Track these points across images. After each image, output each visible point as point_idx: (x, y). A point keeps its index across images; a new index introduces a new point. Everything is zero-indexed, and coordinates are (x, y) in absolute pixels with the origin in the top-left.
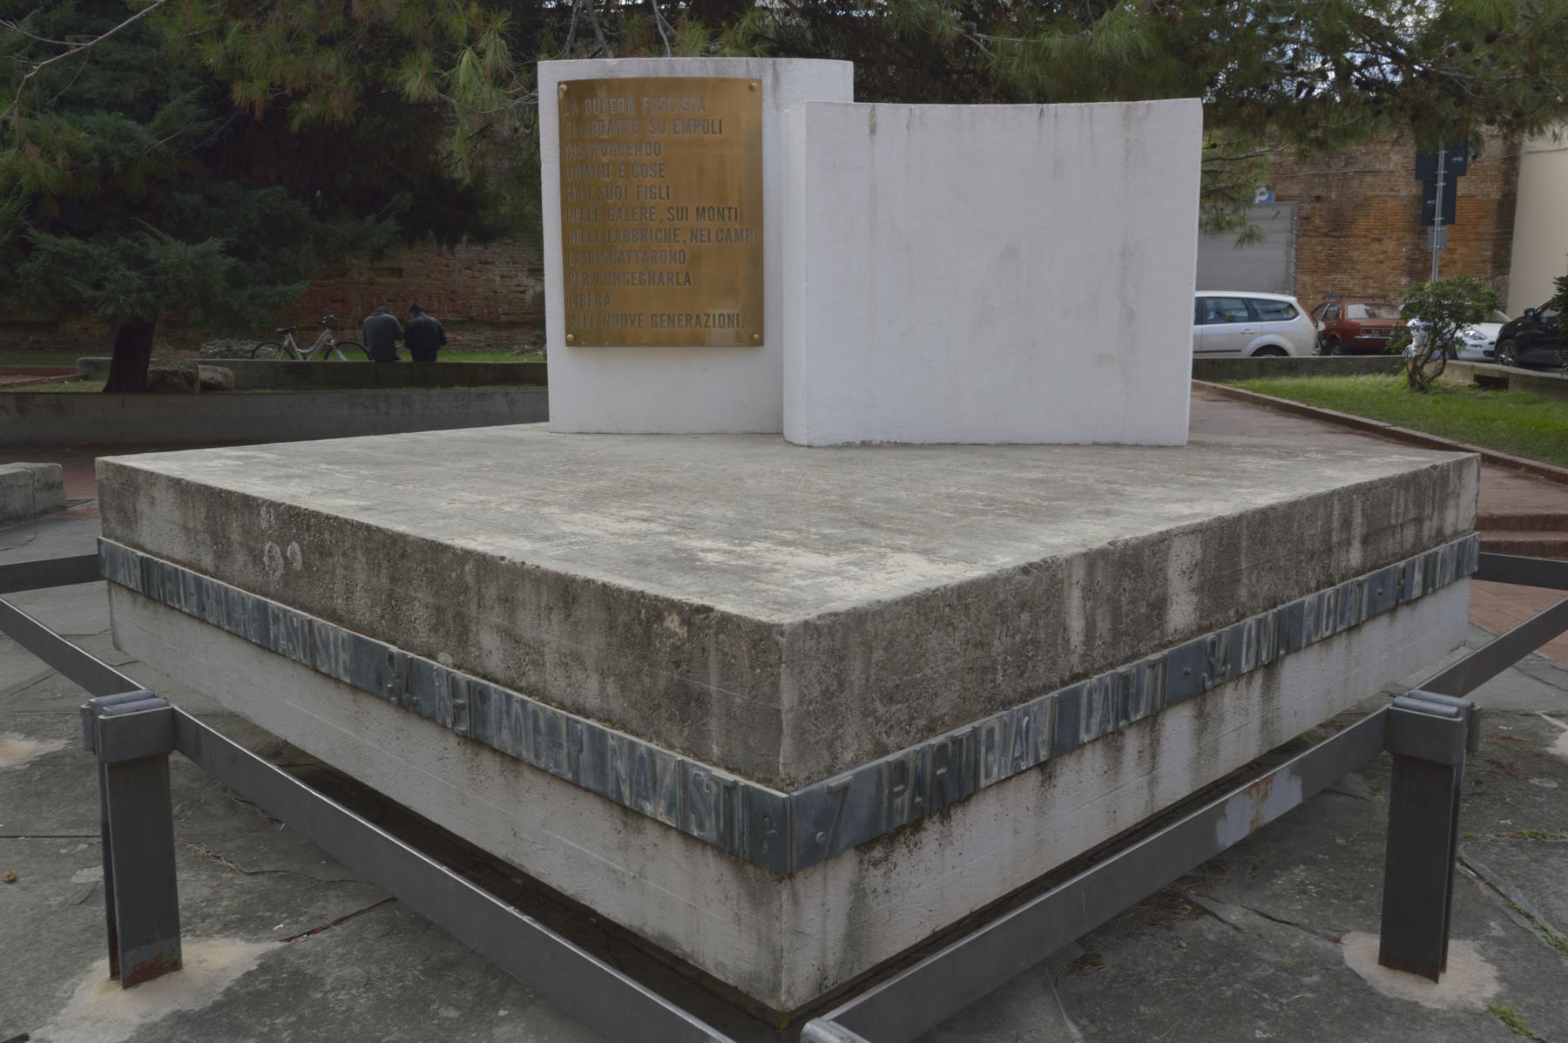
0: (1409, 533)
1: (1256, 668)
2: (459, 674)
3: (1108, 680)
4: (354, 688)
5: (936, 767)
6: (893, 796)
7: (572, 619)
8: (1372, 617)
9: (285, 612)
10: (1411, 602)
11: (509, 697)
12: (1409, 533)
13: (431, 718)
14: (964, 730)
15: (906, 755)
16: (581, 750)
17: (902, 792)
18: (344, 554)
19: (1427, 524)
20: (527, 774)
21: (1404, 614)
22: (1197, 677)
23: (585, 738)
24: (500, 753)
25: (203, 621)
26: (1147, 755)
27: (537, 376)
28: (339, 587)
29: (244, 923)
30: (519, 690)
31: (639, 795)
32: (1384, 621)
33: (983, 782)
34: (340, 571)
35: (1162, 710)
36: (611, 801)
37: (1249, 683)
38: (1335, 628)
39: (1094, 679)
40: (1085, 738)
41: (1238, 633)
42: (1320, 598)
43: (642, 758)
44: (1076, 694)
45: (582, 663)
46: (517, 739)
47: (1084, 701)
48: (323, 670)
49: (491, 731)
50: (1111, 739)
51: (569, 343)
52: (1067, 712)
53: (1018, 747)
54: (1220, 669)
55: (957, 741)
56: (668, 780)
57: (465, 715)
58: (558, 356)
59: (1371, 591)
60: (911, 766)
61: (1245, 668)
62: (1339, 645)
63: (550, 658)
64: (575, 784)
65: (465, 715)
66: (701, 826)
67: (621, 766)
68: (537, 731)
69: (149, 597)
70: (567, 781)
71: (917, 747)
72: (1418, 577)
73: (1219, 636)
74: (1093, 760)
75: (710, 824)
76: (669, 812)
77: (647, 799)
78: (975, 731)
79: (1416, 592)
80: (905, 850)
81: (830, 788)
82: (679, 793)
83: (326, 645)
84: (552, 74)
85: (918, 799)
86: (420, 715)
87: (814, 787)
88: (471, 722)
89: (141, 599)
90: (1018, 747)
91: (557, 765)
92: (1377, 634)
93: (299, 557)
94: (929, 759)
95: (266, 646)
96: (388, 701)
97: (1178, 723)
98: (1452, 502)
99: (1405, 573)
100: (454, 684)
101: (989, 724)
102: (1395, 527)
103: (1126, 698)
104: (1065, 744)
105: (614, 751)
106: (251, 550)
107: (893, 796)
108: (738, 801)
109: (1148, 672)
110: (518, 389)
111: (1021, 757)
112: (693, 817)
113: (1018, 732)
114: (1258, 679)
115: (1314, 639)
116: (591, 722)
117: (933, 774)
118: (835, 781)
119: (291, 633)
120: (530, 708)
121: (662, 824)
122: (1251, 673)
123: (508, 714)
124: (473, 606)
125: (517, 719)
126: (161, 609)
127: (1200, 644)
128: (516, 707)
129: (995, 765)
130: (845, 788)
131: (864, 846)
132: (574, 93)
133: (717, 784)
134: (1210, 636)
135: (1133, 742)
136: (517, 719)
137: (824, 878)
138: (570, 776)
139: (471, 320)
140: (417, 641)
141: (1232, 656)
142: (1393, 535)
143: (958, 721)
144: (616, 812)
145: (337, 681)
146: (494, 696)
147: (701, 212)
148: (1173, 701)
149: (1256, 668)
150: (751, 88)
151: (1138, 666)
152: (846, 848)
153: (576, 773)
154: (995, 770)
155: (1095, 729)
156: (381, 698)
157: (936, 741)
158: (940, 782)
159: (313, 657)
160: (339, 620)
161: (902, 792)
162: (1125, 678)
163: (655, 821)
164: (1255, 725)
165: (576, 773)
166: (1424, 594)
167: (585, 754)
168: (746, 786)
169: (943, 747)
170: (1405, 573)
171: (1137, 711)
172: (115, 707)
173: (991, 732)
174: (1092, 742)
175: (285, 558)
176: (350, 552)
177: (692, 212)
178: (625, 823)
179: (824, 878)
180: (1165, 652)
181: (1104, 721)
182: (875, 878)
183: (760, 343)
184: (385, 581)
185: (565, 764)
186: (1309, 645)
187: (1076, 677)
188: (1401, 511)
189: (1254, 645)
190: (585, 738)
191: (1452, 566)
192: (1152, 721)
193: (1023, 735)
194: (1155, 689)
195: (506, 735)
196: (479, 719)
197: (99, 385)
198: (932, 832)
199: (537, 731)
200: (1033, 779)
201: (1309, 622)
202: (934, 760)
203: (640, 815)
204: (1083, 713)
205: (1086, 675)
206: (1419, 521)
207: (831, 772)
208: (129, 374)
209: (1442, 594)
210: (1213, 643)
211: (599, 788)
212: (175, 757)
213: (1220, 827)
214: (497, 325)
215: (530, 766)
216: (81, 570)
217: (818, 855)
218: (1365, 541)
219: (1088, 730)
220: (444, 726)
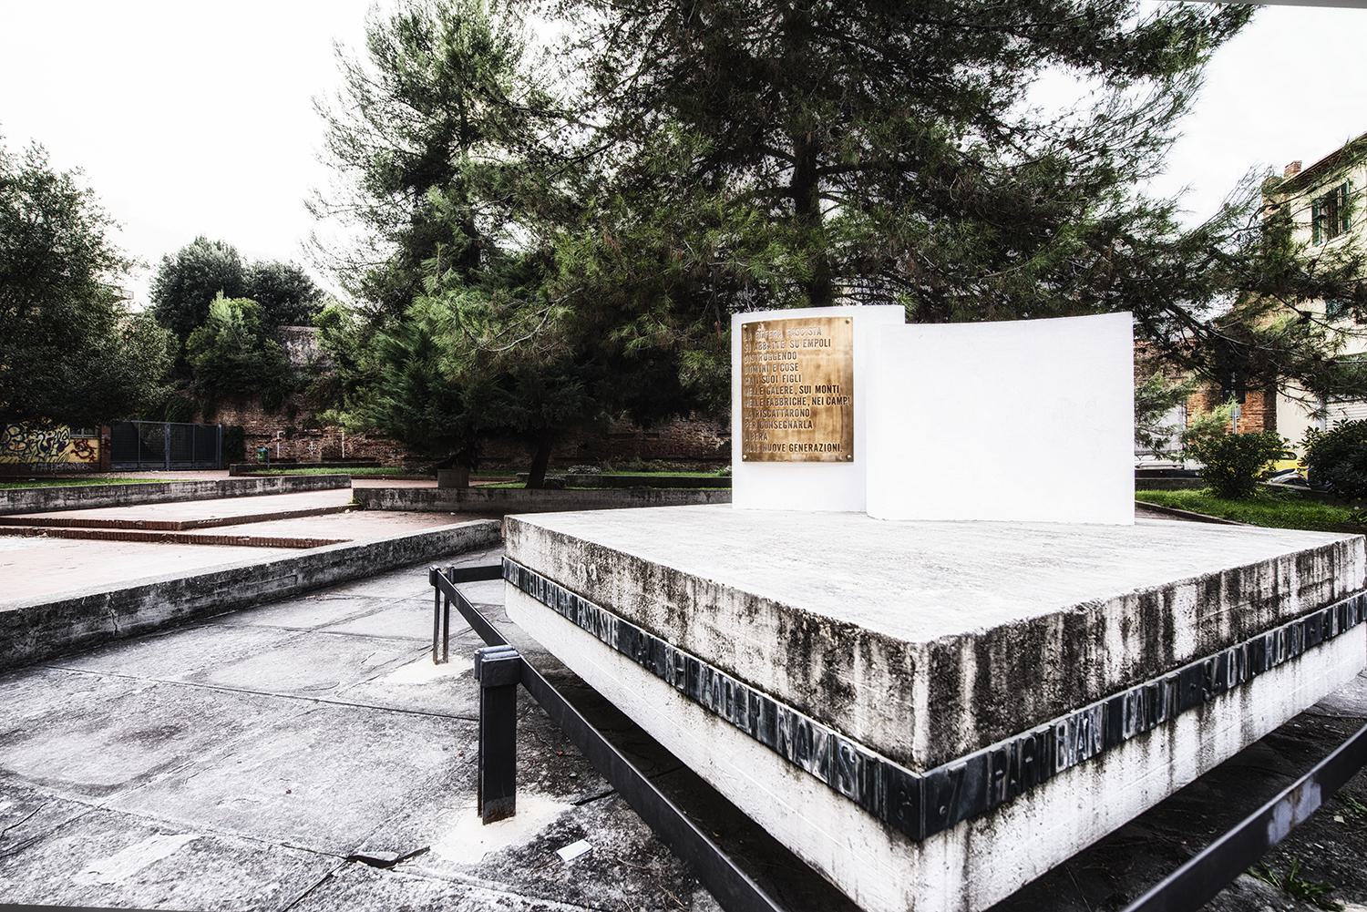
0: (1326, 588)
1: (1237, 685)
2: (681, 652)
3: (1140, 693)
4: (619, 652)
5: (1025, 756)
6: (995, 778)
7: (754, 624)
8: (1308, 649)
9: (586, 604)
10: (1331, 639)
11: (711, 671)
12: (1326, 588)
13: (663, 678)
14: (1043, 728)
15: (1003, 747)
16: (758, 715)
17: (1001, 776)
18: (619, 573)
19: (1336, 583)
20: (720, 723)
21: (1327, 646)
22: (1197, 690)
23: (761, 707)
24: (705, 708)
25: (546, 605)
26: (1167, 748)
27: (726, 482)
28: (615, 592)
29: (556, 787)
30: (719, 667)
31: (799, 754)
32: (1315, 651)
33: (1058, 769)
34: (616, 582)
35: (1178, 715)
36: (778, 754)
37: (1231, 696)
38: (1286, 656)
39: (1130, 691)
40: (1126, 736)
41: (1224, 657)
42: (1276, 634)
43: (801, 726)
44: (1120, 700)
45: (760, 654)
46: (715, 701)
47: (1125, 702)
48: (604, 640)
49: (699, 693)
50: (1143, 736)
51: (744, 460)
52: (1114, 716)
53: (1081, 741)
54: (1214, 685)
55: (1039, 736)
56: (821, 747)
57: (683, 678)
58: (740, 470)
59: (1307, 630)
60: (1008, 754)
61: (1230, 685)
62: (1288, 668)
63: (739, 649)
64: (754, 737)
65: (683, 678)
66: (847, 787)
67: (787, 731)
68: (729, 696)
69: (522, 590)
70: (748, 734)
71: (1012, 740)
72: (1335, 621)
73: (1212, 660)
74: (1132, 751)
75: (854, 786)
76: (822, 771)
77: (805, 758)
78: (1052, 729)
79: (1335, 632)
80: (1002, 820)
81: (950, 772)
82: (831, 759)
83: (606, 625)
84: (739, 320)
85: (1013, 782)
86: (656, 674)
87: (938, 770)
88: (688, 678)
89: (519, 590)
90: (1081, 741)
91: (742, 722)
92: (1311, 659)
93: (595, 573)
94: (1020, 750)
95: (575, 620)
96: (638, 663)
97: (1187, 722)
98: (1350, 568)
99: (1329, 617)
100: (677, 657)
101: (1060, 725)
102: (1316, 585)
103: (1153, 705)
104: (1113, 740)
105: (782, 719)
106: (571, 567)
107: (995, 778)
108: (878, 773)
109: (1166, 686)
110: (719, 488)
111: (1083, 750)
112: (841, 779)
113: (1081, 730)
114: (1238, 694)
115: (1274, 664)
116: (766, 696)
117: (1024, 762)
118: (955, 765)
119: (589, 616)
120: (725, 680)
121: (816, 778)
122: (1233, 688)
123: (710, 683)
124: (691, 609)
125: (716, 687)
126: (527, 596)
127: (1201, 665)
128: (715, 679)
129: (1067, 755)
130: (961, 771)
131: (972, 818)
132: (751, 329)
133: (861, 757)
134: (1206, 660)
135: (1158, 737)
136: (716, 687)
137: (946, 842)
138: (750, 731)
139: (690, 458)
140: (657, 628)
141: (1222, 676)
142: (1316, 590)
143: (1040, 719)
144: (781, 762)
145: (611, 647)
146: (702, 669)
147: (818, 389)
148: (1184, 709)
149: (1237, 685)
150: (847, 322)
151: (1160, 682)
152: (961, 820)
153: (754, 730)
154: (1065, 759)
155: (1132, 732)
156: (634, 661)
157: (1026, 735)
158: (1026, 766)
159: (599, 632)
160: (614, 611)
161: (1001, 776)
162: (1151, 689)
163: (811, 774)
164: (1238, 726)
165: (754, 730)
166: (1340, 632)
167: (760, 718)
168: (885, 763)
169: (1030, 740)
170: (1329, 617)
171: (1161, 716)
172: (493, 654)
173: (1062, 730)
174: (1131, 739)
175: (588, 572)
176: (622, 571)
177: (813, 389)
178: (788, 771)
179: (946, 842)
180: (1178, 671)
181: (1139, 722)
182: (979, 841)
183: (851, 460)
184: (640, 590)
185: (747, 722)
186: (1270, 668)
187: (1118, 689)
188: (1320, 573)
189: (1235, 668)
190: (761, 707)
191: (1355, 613)
192: (1171, 724)
193: (1084, 733)
194: (1172, 698)
195: (708, 697)
196: (692, 683)
197: (523, 485)
198: (1022, 804)
199: (729, 696)
200: (1090, 767)
201: (1269, 651)
202: (1023, 751)
203: (800, 768)
204: (1124, 717)
205: (1125, 688)
206: (1331, 581)
207: (950, 758)
208: (535, 482)
209: (1349, 633)
210: (1209, 665)
211: (771, 744)
212: (520, 687)
213: (1271, 828)
214: (701, 460)
215: (723, 718)
216: (494, 573)
217: (940, 825)
218: (1299, 594)
219: (1128, 731)
220: (670, 684)
